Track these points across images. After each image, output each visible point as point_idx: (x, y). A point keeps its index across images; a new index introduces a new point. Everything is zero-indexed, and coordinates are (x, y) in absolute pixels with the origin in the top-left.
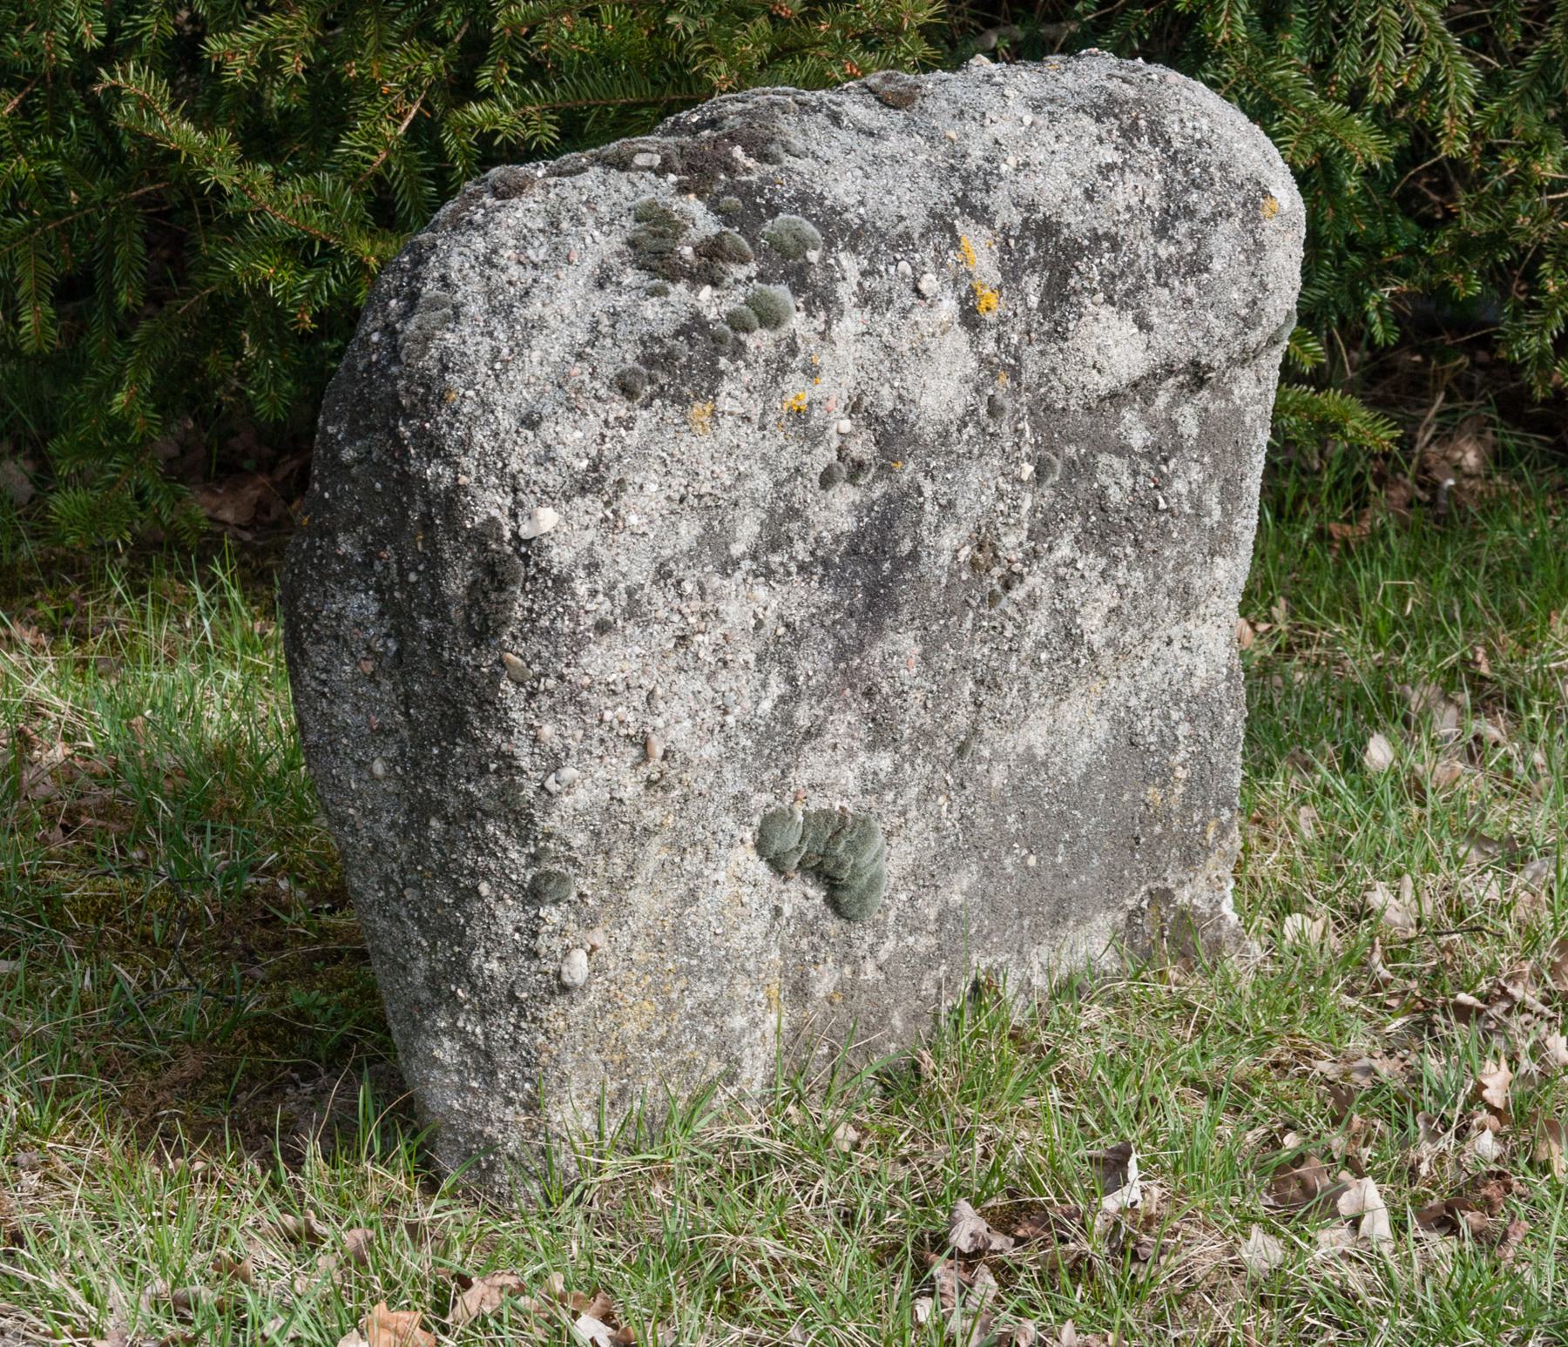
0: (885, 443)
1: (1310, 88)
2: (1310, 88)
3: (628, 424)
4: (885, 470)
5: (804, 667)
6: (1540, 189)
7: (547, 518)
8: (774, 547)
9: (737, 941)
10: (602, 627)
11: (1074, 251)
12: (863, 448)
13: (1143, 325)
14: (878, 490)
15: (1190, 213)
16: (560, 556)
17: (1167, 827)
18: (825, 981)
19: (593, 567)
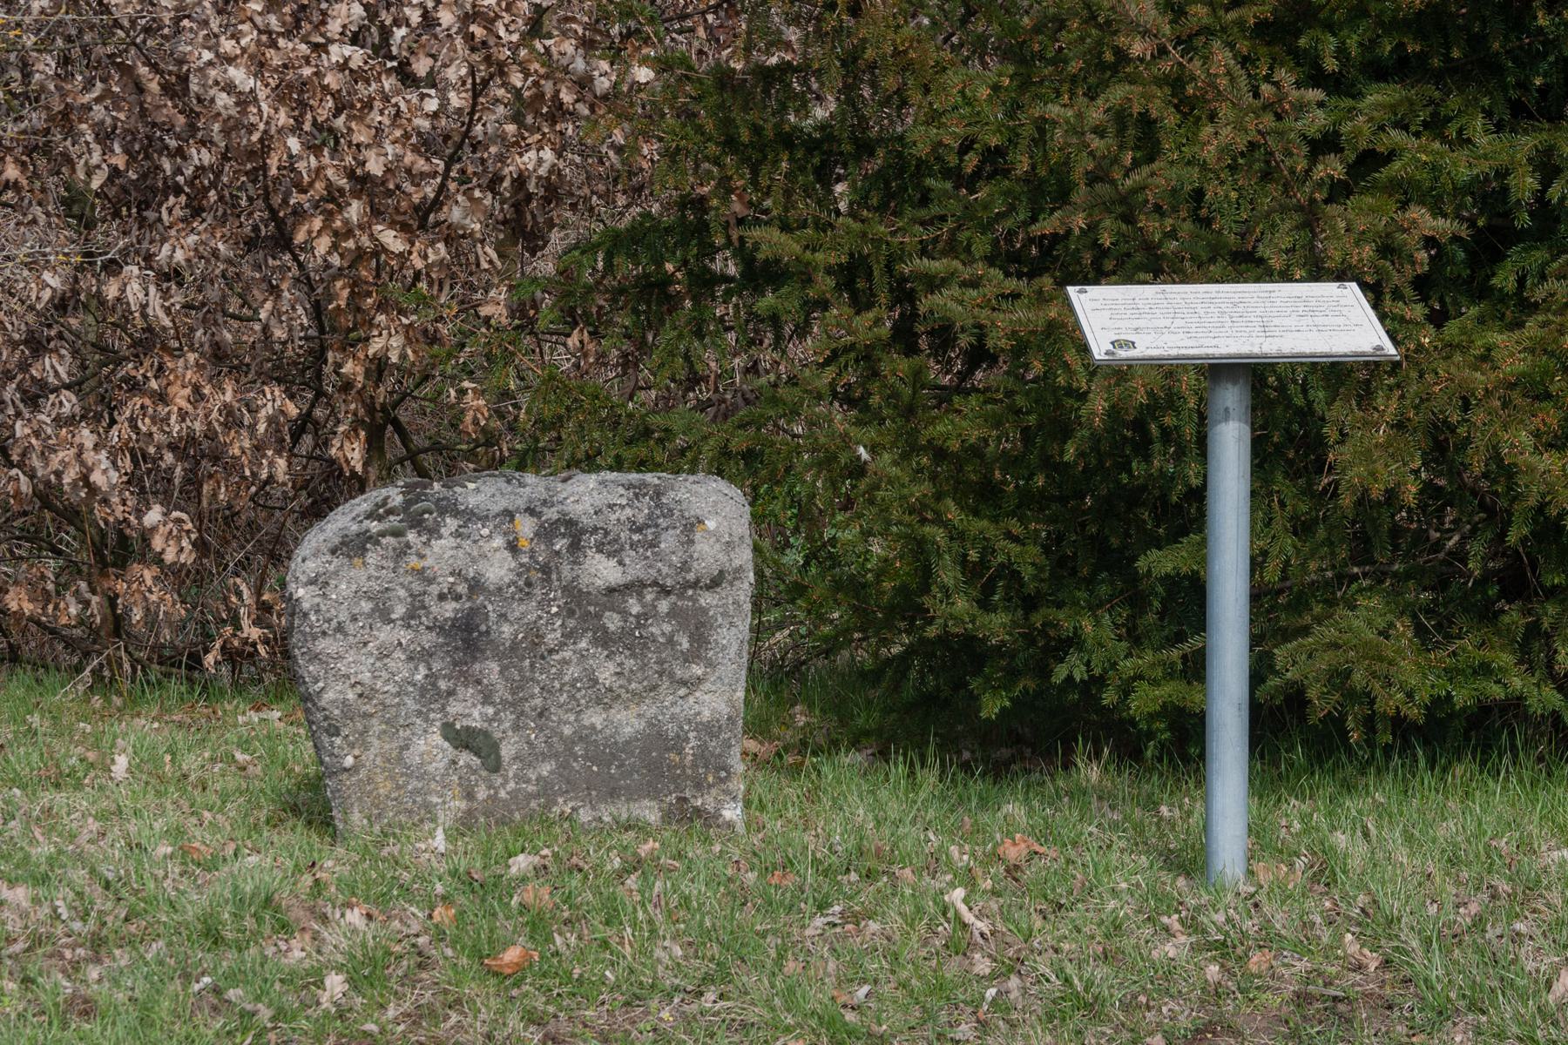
0: (471, 588)
1: (1454, 776)
2: (1454, 776)
3: (330, 563)
4: (470, 598)
5: (436, 666)
6: (83, 367)
7: (301, 592)
8: (413, 618)
9: (431, 768)
10: (324, 633)
11: (583, 531)
12: (462, 588)
13: (621, 563)
14: (468, 605)
15: (657, 526)
16: (306, 606)
17: (684, 771)
18: (482, 793)
19: (317, 611)
